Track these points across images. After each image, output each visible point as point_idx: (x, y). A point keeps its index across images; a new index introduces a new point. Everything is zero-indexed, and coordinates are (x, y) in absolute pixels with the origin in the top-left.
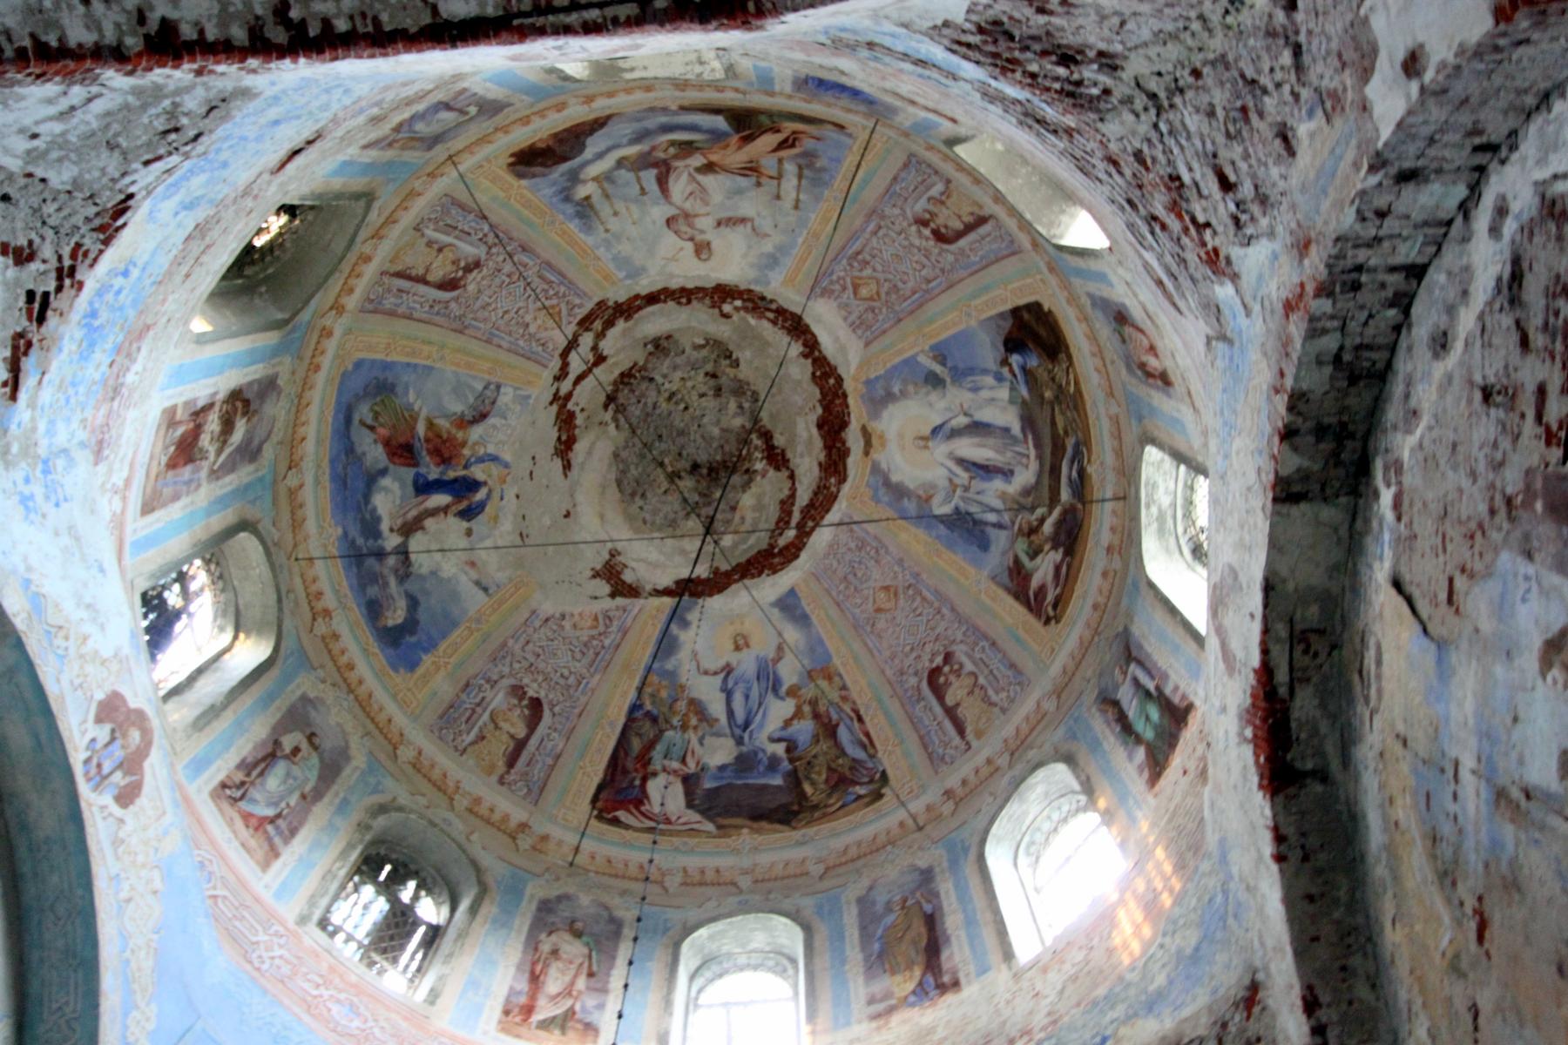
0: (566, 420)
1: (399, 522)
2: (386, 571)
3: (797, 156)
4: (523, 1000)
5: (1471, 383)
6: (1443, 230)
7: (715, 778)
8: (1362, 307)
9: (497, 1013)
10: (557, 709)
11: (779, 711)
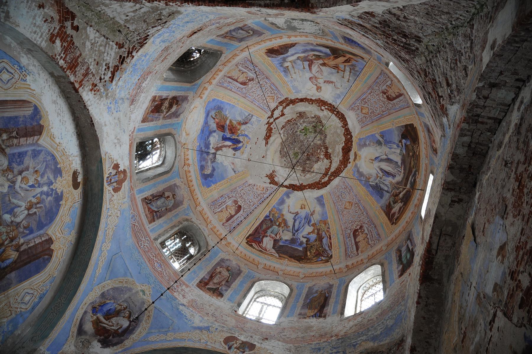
0: (270, 131)
1: (216, 146)
2: (208, 159)
3: (349, 65)
4: (206, 281)
5: (503, 159)
6: (507, 108)
7: (283, 243)
8: (479, 130)
9: (198, 282)
10: (245, 210)
11: (308, 229)
